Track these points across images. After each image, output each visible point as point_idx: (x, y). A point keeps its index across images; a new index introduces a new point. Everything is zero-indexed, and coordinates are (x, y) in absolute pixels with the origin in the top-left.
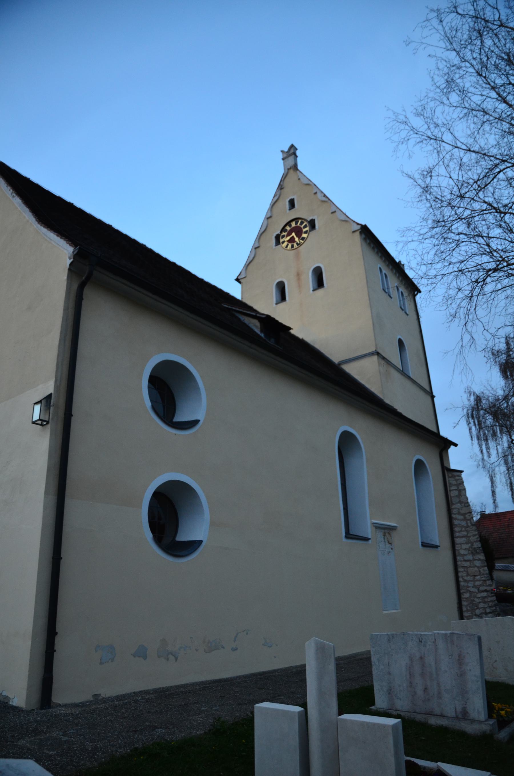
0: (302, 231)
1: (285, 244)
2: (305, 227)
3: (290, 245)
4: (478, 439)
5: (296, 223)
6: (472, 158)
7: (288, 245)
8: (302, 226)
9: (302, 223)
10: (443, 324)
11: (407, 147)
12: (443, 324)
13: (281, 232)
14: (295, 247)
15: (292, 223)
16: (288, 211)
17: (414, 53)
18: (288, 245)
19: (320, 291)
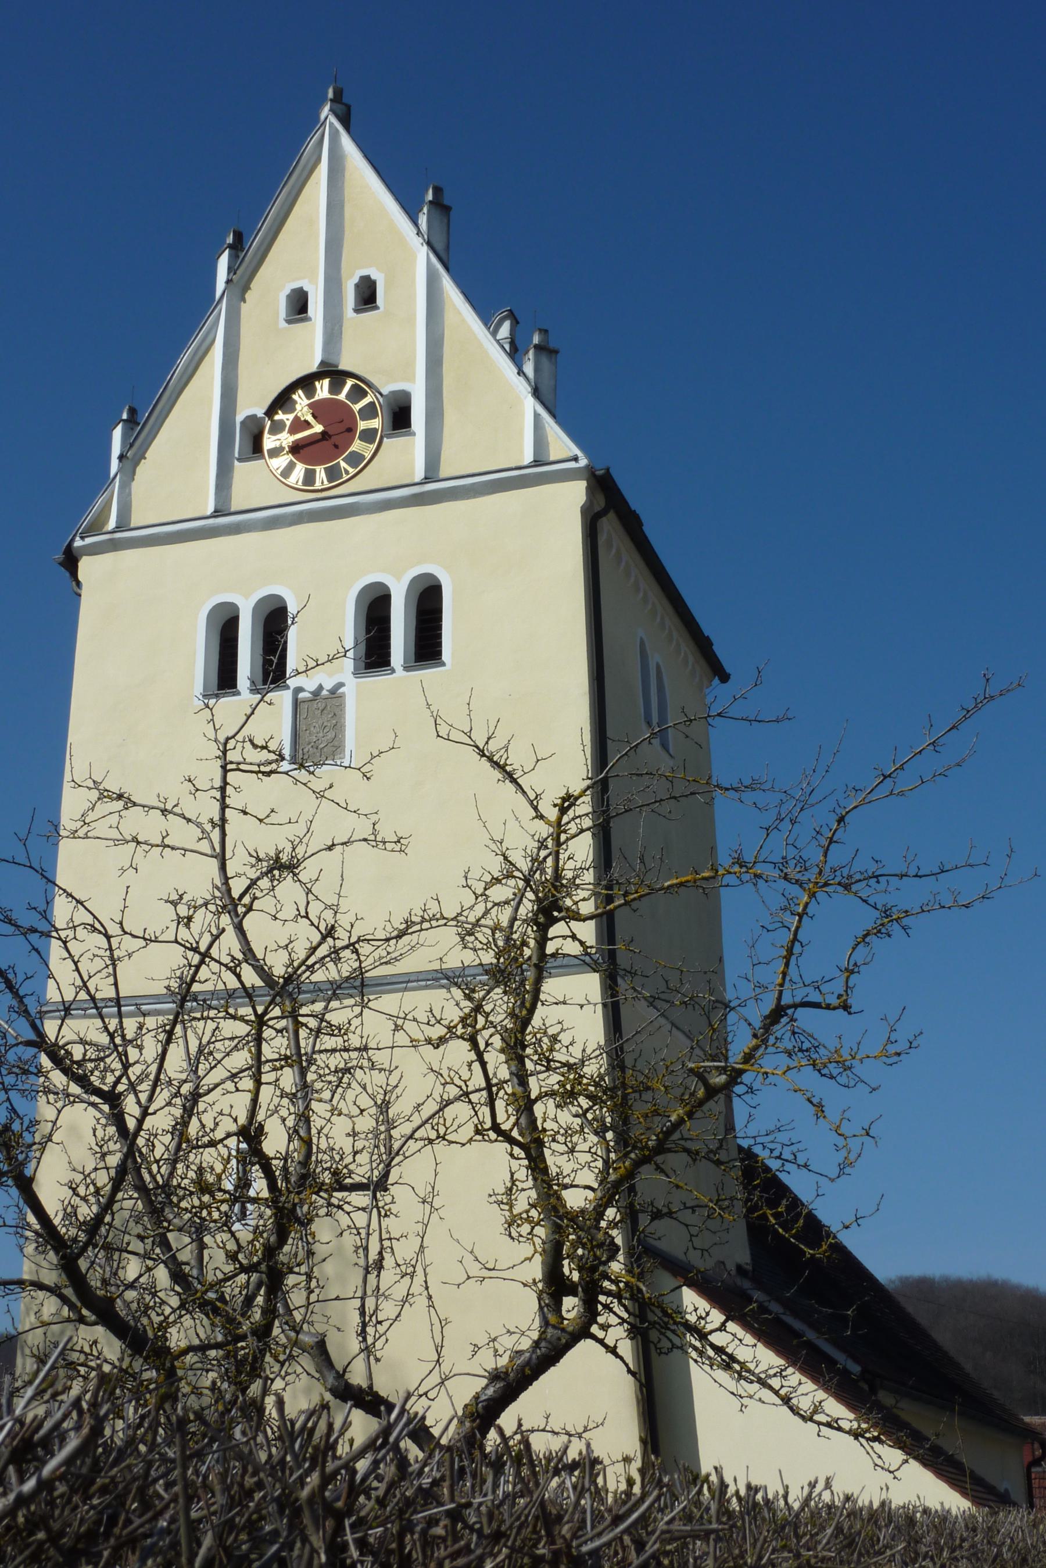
0: (351, 430)
1: (280, 462)
2: (369, 412)
3: (300, 470)
4: (607, 1491)
5: (335, 388)
6: (117, 1428)
7: (291, 467)
8: (357, 407)
9: (358, 393)
10: (232, 1107)
11: (294, 849)
12: (232, 1107)
13: (270, 412)
14: (318, 485)
15: (295, 397)
16: (283, 324)
17: (339, 1329)
18: (291, 467)
19: (429, 674)
